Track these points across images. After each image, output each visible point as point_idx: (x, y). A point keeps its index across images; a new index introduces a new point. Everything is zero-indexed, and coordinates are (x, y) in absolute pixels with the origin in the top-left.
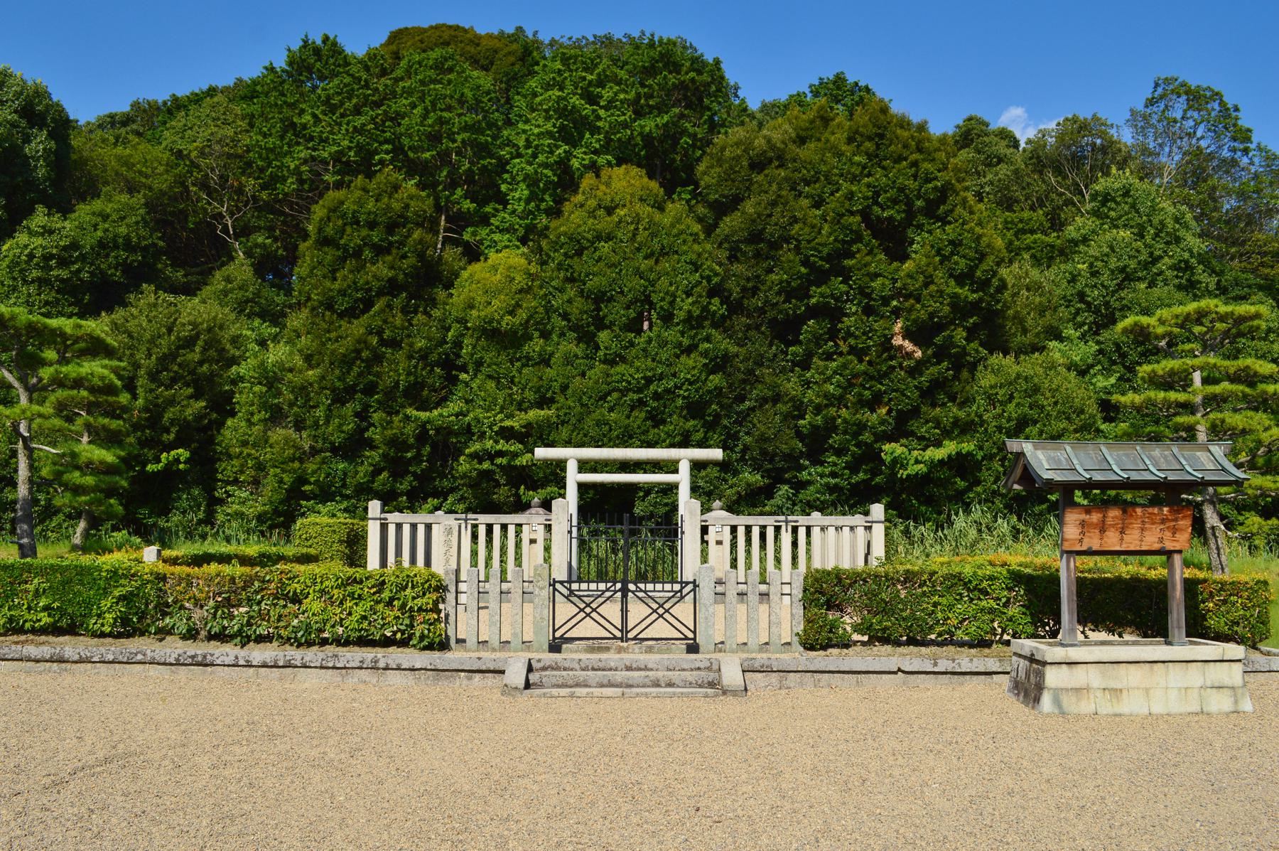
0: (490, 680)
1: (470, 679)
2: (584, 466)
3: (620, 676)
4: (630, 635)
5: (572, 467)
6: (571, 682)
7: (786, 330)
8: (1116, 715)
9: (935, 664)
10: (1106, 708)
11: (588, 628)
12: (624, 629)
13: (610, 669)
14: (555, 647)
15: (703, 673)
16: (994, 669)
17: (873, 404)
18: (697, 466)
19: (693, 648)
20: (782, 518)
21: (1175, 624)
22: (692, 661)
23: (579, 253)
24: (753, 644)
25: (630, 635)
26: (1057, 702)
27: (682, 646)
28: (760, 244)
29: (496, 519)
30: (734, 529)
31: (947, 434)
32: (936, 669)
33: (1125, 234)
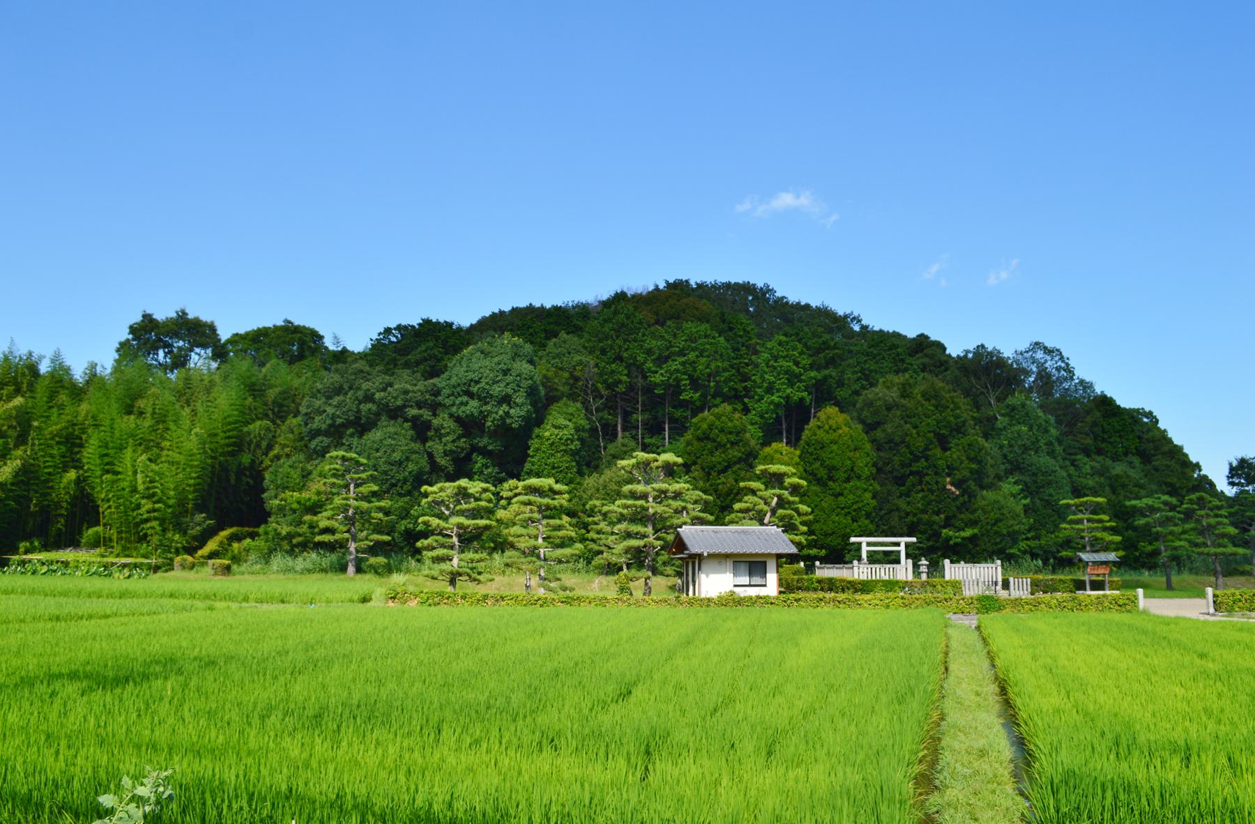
2: (869, 544)
5: (864, 545)
7: (900, 480)
17: (938, 514)
21: (1127, 577)
23: (823, 447)
28: (891, 444)
29: (878, 566)
31: (966, 525)
33: (1024, 429)
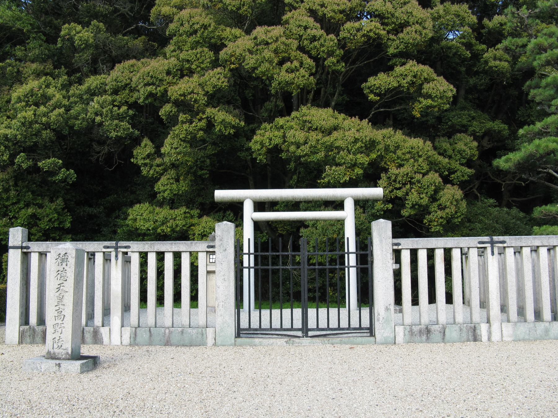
2: (260, 206)
5: (248, 207)
18: (359, 203)
20: (486, 239)
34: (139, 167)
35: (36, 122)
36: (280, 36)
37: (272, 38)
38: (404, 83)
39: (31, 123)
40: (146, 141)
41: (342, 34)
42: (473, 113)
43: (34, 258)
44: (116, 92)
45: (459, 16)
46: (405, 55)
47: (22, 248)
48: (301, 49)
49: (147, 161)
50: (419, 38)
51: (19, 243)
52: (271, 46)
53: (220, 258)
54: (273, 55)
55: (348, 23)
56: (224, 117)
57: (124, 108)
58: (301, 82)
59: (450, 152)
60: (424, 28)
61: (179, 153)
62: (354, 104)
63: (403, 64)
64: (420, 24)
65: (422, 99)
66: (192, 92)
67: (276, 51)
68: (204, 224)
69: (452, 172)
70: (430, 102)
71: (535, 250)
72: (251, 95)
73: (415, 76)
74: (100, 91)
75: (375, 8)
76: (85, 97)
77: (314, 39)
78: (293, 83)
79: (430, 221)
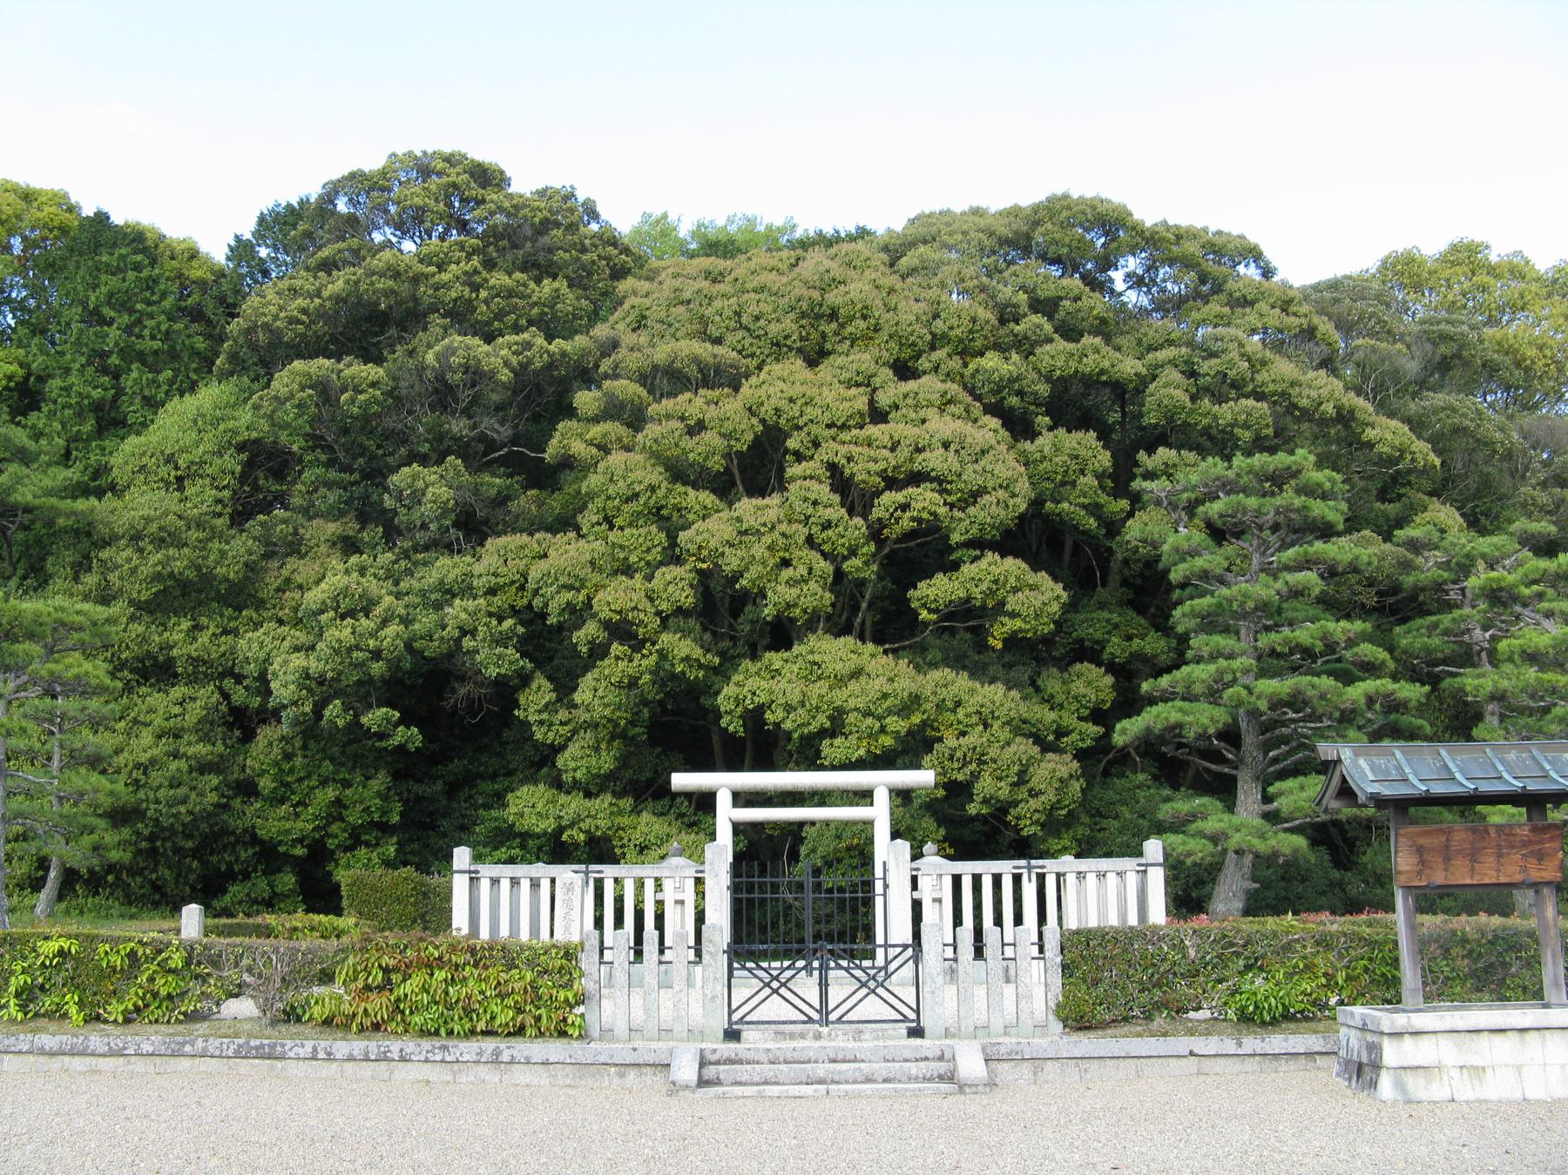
0: (651, 1079)
1: (622, 1075)
2: (743, 798)
3: (822, 1070)
4: (833, 1017)
5: (724, 802)
6: (756, 1079)
8: (1480, 1101)
9: (1240, 1045)
10: (1466, 1091)
11: (775, 1008)
12: (824, 1009)
13: (809, 1062)
14: (732, 1035)
15: (933, 1065)
16: (1317, 1049)
18: (902, 796)
19: (917, 1032)
20: (1023, 863)
22: (917, 1048)
24: (997, 1024)
25: (833, 1017)
26: (1400, 1086)
27: (902, 1029)
30: (957, 880)
32: (1240, 1052)
34: (529, 725)
35: (357, 647)
36: (780, 522)
37: (764, 525)
38: (976, 593)
39: (350, 650)
40: (540, 681)
41: (877, 513)
42: (1115, 618)
43: (485, 885)
44: (492, 592)
45: (1077, 457)
46: (979, 545)
47: (470, 872)
48: (810, 541)
49: (545, 716)
50: (1003, 513)
51: (466, 867)
52: (764, 539)
53: (693, 884)
54: (767, 554)
55: (887, 493)
56: (682, 647)
57: (509, 623)
58: (809, 602)
59: (1059, 698)
60: (1014, 495)
61: (606, 706)
62: (892, 626)
63: (975, 559)
64: (1006, 488)
65: (1006, 620)
66: (635, 608)
67: (770, 548)
68: (642, 828)
69: (1060, 733)
70: (1018, 623)
71: (1102, 875)
72: (728, 613)
73: (996, 582)
74: (464, 589)
75: (931, 465)
76: (433, 597)
77: (827, 525)
78: (795, 605)
79: (1018, 818)
